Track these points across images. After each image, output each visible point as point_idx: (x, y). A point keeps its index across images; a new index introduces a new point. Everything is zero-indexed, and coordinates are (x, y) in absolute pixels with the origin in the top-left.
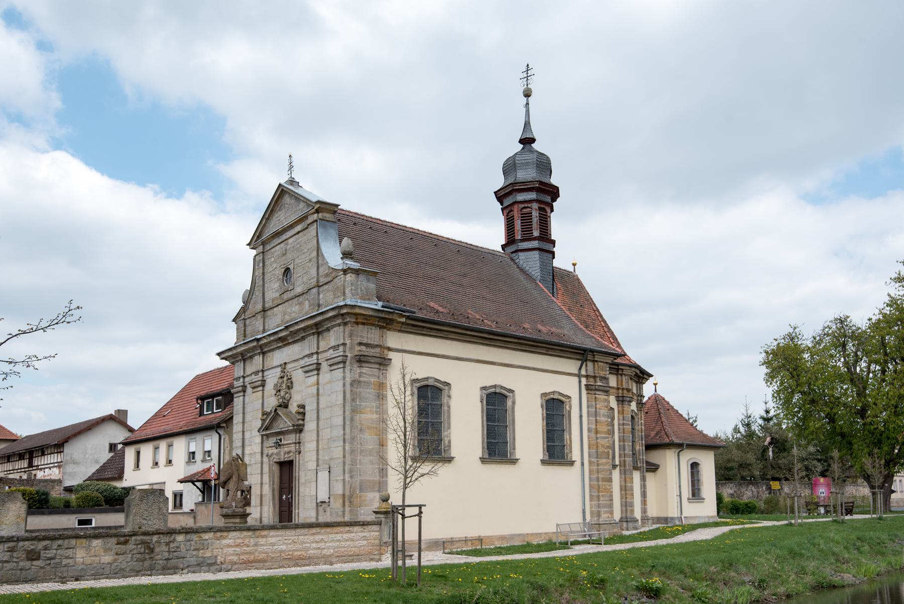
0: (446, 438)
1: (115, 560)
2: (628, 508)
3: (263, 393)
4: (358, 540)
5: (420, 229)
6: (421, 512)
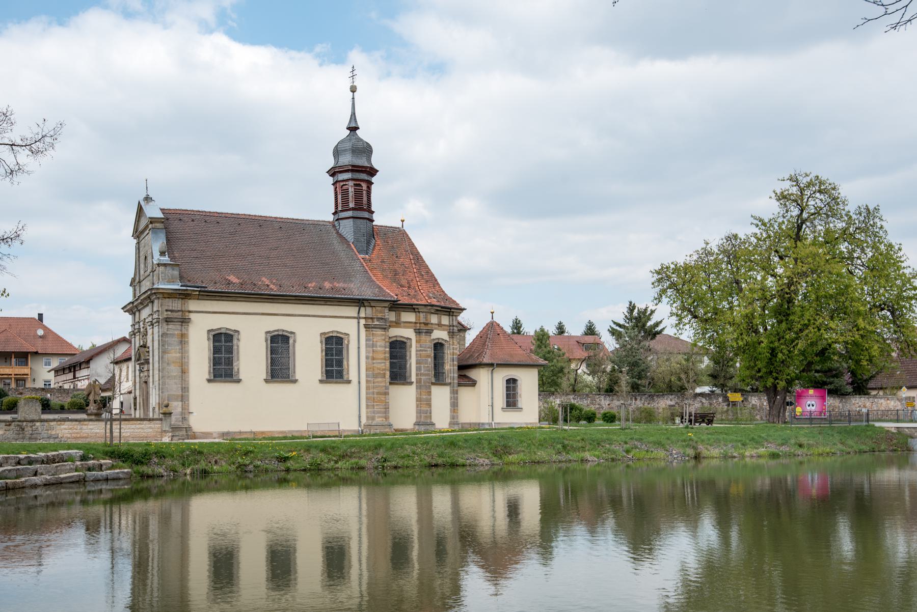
1: (5, 434)
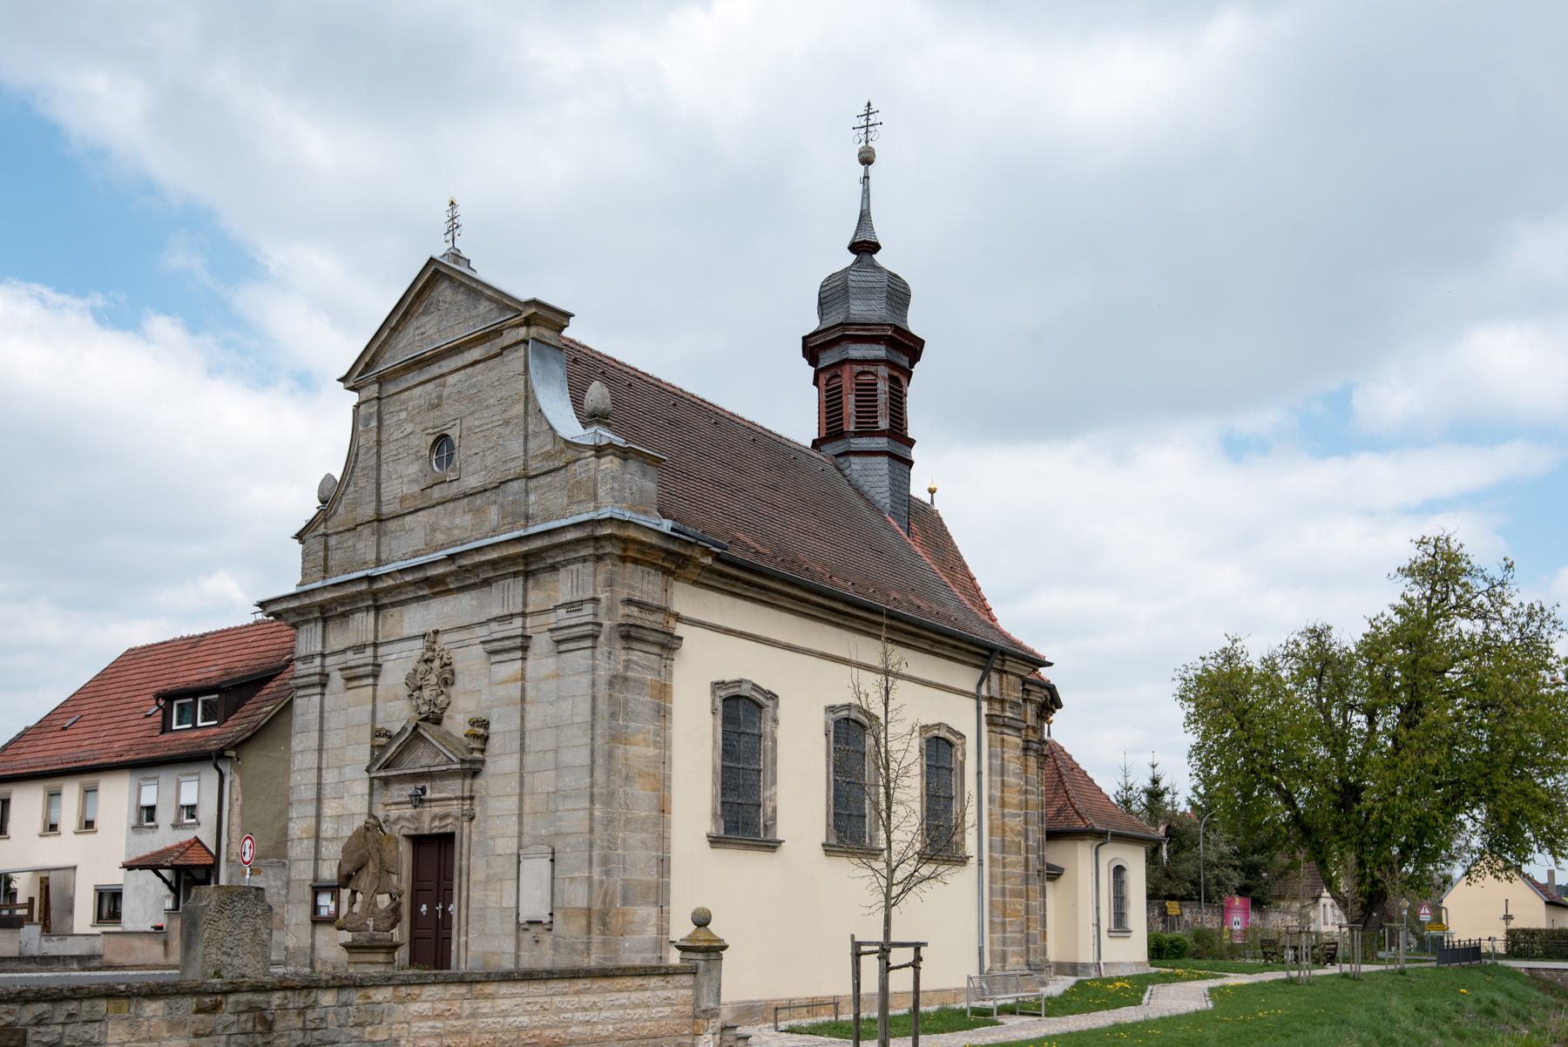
0: (768, 802)
2: (1031, 946)
3: (375, 691)
4: (658, 1005)
5: (685, 389)
6: (918, 958)
